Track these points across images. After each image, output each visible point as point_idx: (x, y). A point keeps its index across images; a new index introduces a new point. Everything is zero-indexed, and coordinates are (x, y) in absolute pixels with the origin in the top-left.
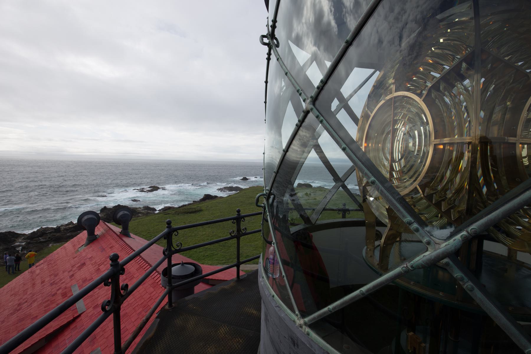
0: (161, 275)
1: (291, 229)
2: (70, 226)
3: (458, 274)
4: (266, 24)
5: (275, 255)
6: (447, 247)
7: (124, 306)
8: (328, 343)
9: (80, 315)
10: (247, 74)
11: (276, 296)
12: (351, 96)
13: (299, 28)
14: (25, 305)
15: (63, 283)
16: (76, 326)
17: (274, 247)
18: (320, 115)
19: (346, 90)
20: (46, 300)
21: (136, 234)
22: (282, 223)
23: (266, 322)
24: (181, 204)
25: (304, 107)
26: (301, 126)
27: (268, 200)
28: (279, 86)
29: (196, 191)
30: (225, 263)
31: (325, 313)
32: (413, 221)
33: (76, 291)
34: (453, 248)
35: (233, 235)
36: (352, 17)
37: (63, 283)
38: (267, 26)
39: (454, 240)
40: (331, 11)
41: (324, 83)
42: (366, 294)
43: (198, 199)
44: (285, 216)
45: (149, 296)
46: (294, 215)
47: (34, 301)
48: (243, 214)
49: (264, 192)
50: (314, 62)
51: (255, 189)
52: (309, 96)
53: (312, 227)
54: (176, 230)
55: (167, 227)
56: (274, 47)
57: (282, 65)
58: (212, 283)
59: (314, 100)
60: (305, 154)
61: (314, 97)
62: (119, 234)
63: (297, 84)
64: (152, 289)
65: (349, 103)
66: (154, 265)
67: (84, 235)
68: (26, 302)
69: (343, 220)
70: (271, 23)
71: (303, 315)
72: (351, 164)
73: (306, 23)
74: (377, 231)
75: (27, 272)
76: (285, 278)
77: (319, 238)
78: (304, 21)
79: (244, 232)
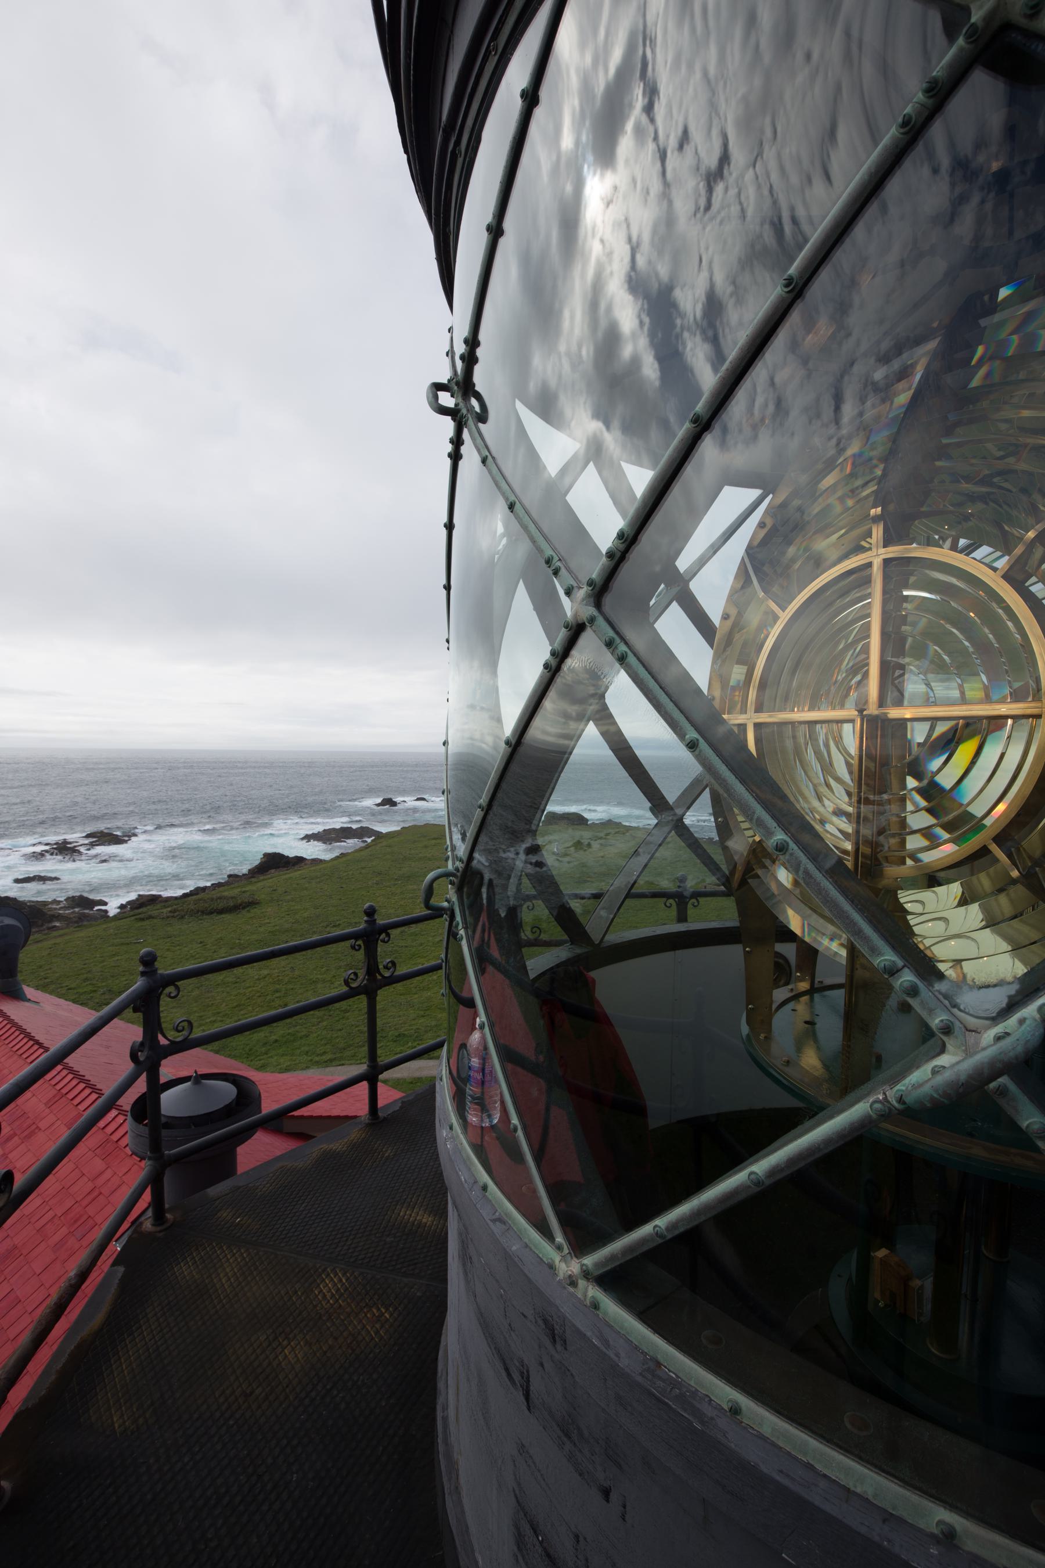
0: (129, 1118)
1: (530, 964)
4: (447, 348)
5: (485, 1059)
8: (656, 1330)
10: (388, 483)
13: (545, 366)
18: (618, 640)
23: (464, 1265)
24: (190, 885)
25: (569, 613)
28: (489, 531)
29: (243, 848)
31: (643, 1241)
32: (900, 963)
34: (1020, 1049)
35: (354, 985)
36: (698, 339)
38: (450, 353)
40: (641, 323)
41: (629, 540)
42: (768, 1182)
43: (244, 869)
44: (513, 912)
45: (90, 1186)
46: (536, 914)
50: (591, 464)
51: (425, 837)
52: (585, 580)
54: (172, 980)
55: (143, 974)
56: (471, 422)
57: (499, 478)
59: (600, 591)
61: (599, 582)
63: (545, 546)
64: (98, 1164)
66: (108, 1091)
69: (682, 927)
70: (460, 348)
71: (582, 1239)
73: (568, 354)
74: (778, 955)
76: (520, 1134)
77: (614, 987)
78: (562, 347)
79: (387, 974)
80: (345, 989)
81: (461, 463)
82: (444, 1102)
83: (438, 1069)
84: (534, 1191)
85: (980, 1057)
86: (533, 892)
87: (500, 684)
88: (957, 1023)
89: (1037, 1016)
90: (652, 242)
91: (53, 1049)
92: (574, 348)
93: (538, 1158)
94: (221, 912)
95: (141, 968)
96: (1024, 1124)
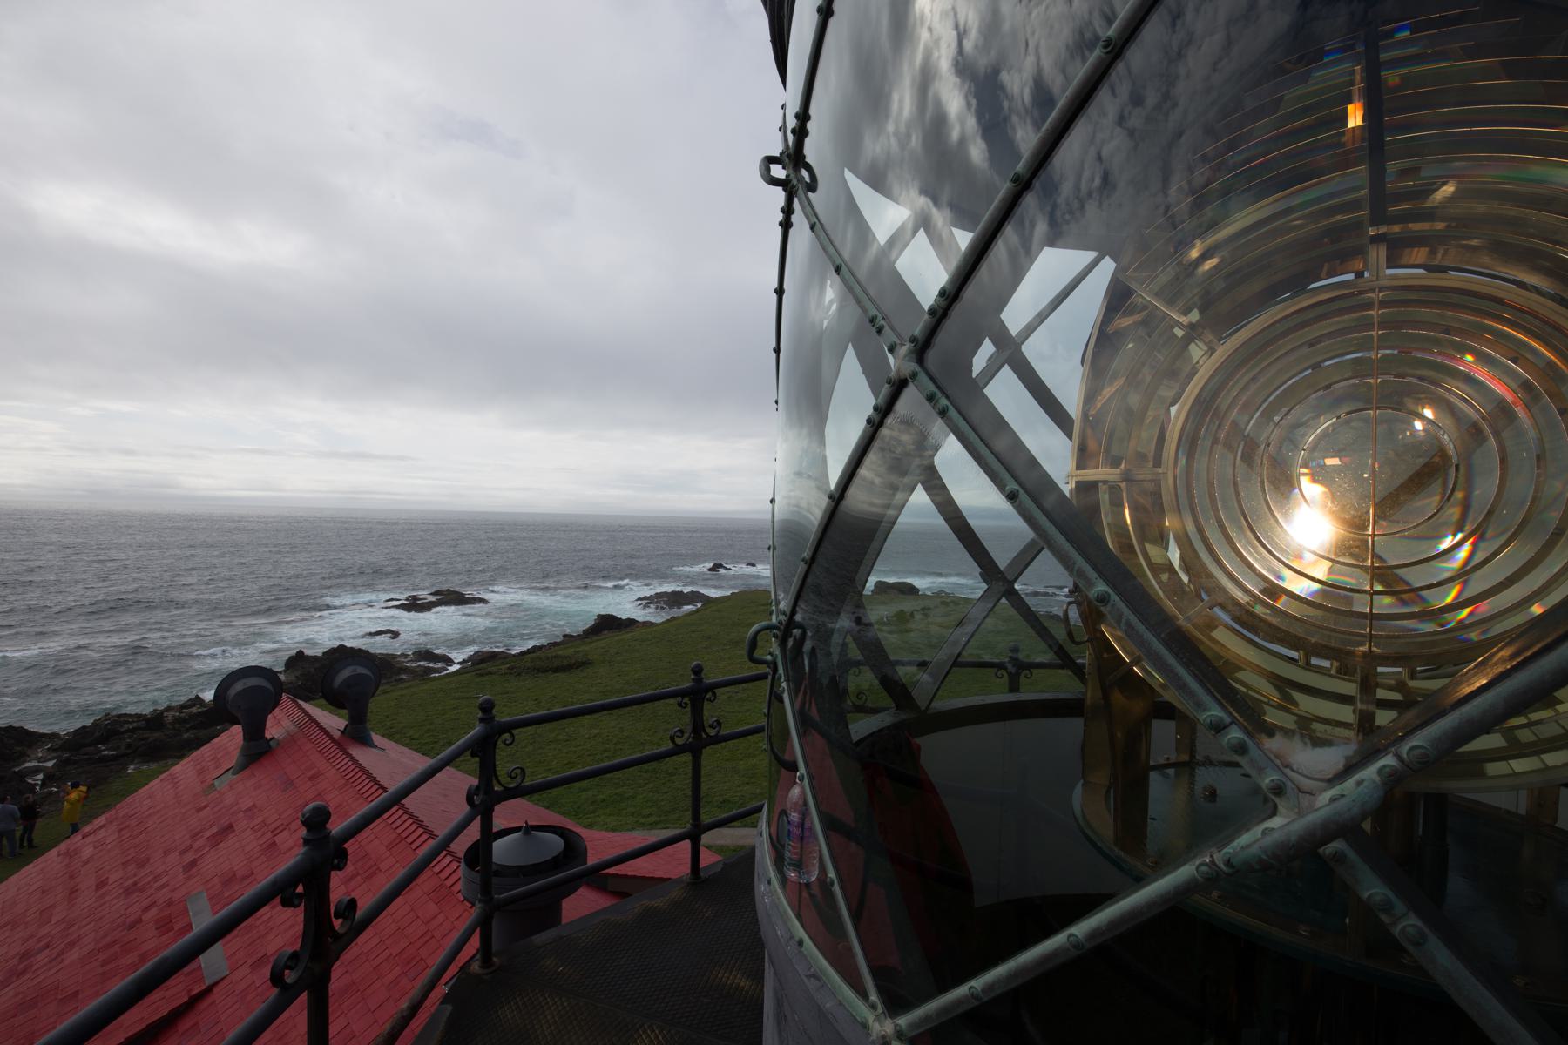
0: (463, 864)
2: (194, 710)
3: (1373, 889)
4: (780, 123)
5: (805, 814)
6: (1336, 805)
7: (339, 977)
9: (208, 991)
11: (807, 941)
12: (1030, 329)
14: (43, 957)
15: (163, 886)
16: (196, 1024)
17: (803, 788)
18: (939, 394)
19: (1015, 316)
20: (107, 940)
21: (389, 736)
22: (826, 700)
23: (779, 1024)
26: (881, 424)
27: (783, 643)
29: (576, 607)
30: (656, 823)
31: (959, 1002)
32: (1228, 720)
33: (203, 919)
35: (679, 741)
37: (163, 886)
38: (783, 128)
39: (1359, 783)
40: (968, 104)
41: (951, 296)
46: (863, 680)
47: (72, 945)
48: (710, 678)
49: (774, 619)
51: (751, 600)
53: (917, 720)
54: (509, 727)
56: (800, 191)
58: (621, 889)
59: (921, 348)
60: (899, 496)
61: (921, 339)
62: (337, 735)
65: (1024, 348)
66: (442, 833)
67: (233, 738)
68: (47, 946)
69: (1012, 697)
70: (792, 123)
71: (895, 1004)
72: (1028, 534)
75: (54, 852)
76: (836, 888)
77: (939, 755)
78: (890, 127)
79: (712, 732)
80: (670, 745)
81: (791, 231)
82: (763, 857)
83: (758, 837)
84: (850, 949)
85: (1311, 818)
86: (860, 658)
87: (828, 453)
88: (1289, 784)
89: (1378, 779)
90: (980, 31)
91: (391, 789)
92: (903, 128)
93: (856, 917)
94: (556, 670)
95: (480, 715)
96: (1366, 895)
